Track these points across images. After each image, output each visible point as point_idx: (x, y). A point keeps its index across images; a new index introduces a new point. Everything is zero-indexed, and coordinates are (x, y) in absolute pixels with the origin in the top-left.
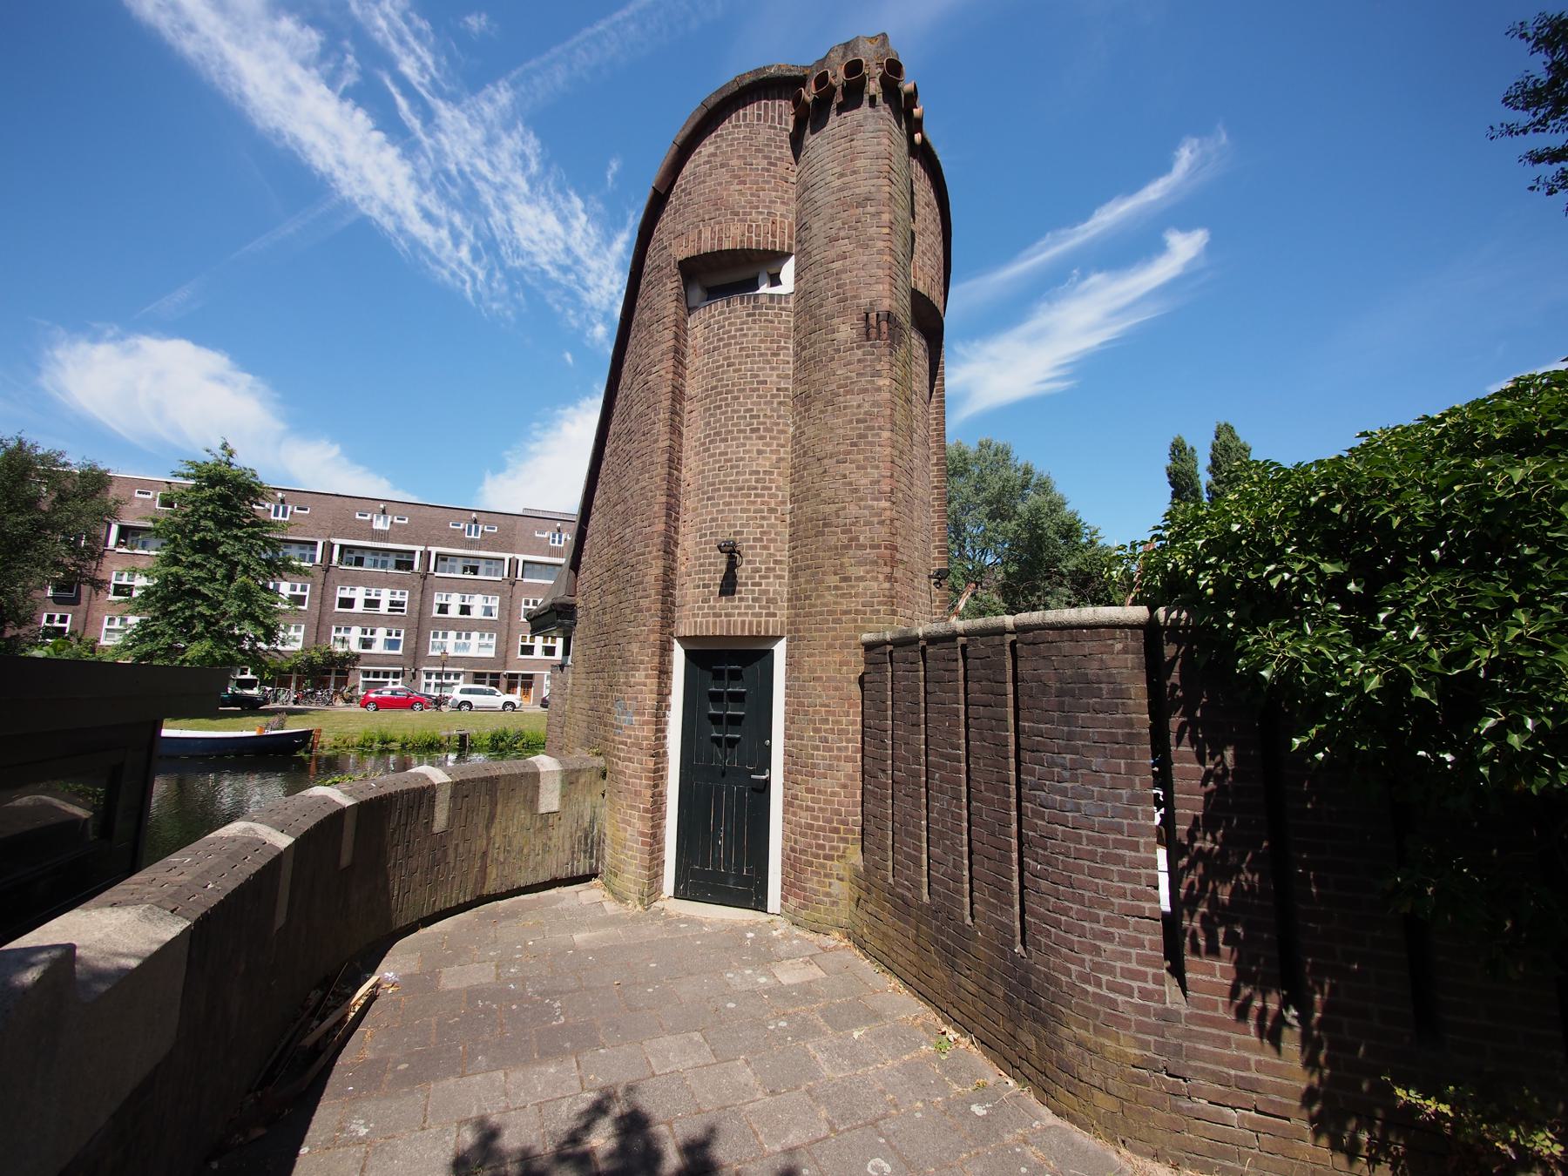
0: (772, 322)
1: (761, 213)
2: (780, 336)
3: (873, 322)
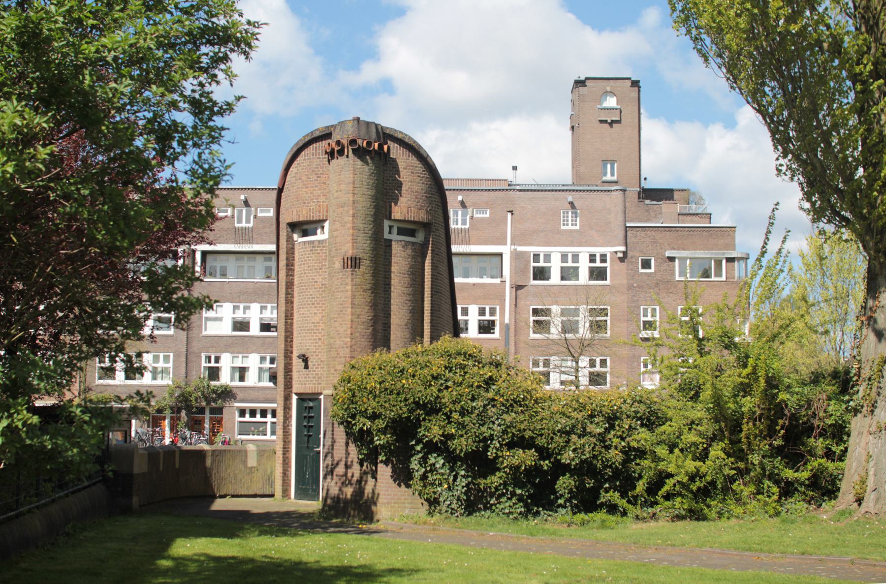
0: (319, 253)
2: (323, 260)
3: (346, 261)
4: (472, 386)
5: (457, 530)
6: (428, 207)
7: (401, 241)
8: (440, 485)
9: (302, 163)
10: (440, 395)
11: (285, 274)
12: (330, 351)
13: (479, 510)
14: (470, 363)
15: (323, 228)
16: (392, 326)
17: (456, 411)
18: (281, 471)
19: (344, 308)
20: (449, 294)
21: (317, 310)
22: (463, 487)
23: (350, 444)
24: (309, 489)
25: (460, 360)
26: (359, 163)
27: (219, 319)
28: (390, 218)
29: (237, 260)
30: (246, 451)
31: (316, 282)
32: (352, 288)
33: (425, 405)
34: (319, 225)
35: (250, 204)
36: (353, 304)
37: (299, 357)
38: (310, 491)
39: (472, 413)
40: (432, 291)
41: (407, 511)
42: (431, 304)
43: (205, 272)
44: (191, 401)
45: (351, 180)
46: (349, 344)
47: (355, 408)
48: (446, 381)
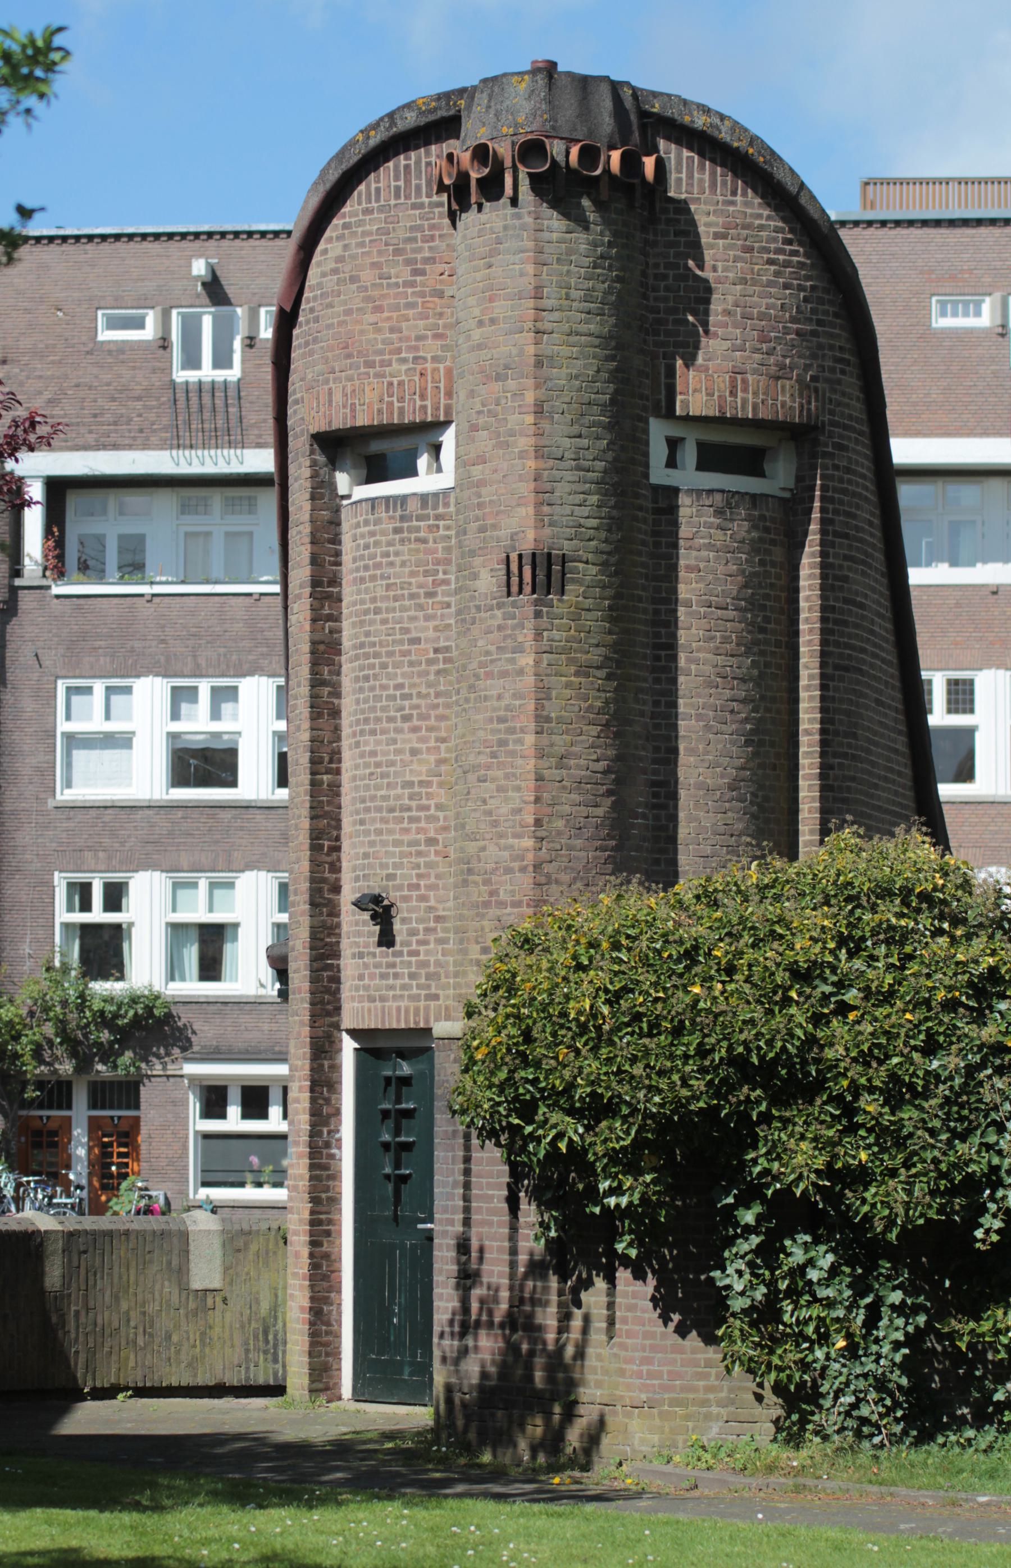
0: (424, 541)
1: (404, 361)
2: (438, 562)
4: (927, 1003)
5: (875, 1489)
6: (807, 368)
7: (710, 492)
8: (824, 1338)
9: (360, 223)
10: (820, 1034)
11: (308, 614)
12: (465, 883)
13: (961, 1422)
14: (925, 921)
15: (436, 449)
16: (682, 793)
17: (871, 1090)
18: (307, 1304)
19: (511, 731)
20: (894, 671)
21: (422, 740)
22: (897, 1345)
23: (524, 1206)
24: (401, 1364)
25: (889, 912)
26: (555, 222)
27: (121, 741)
28: (669, 413)
29: (185, 509)
30: (184, 1236)
31: (417, 641)
32: (537, 663)
33: (768, 1068)
34: (421, 440)
35: (230, 291)
36: (541, 719)
37: (359, 904)
38: (407, 1370)
39: (926, 1095)
40: (823, 665)
41: (715, 1429)
42: (823, 710)
43: (61, 557)
44: (16, 1056)
45: (527, 283)
46: (530, 856)
47: (535, 1082)
48: (841, 985)
